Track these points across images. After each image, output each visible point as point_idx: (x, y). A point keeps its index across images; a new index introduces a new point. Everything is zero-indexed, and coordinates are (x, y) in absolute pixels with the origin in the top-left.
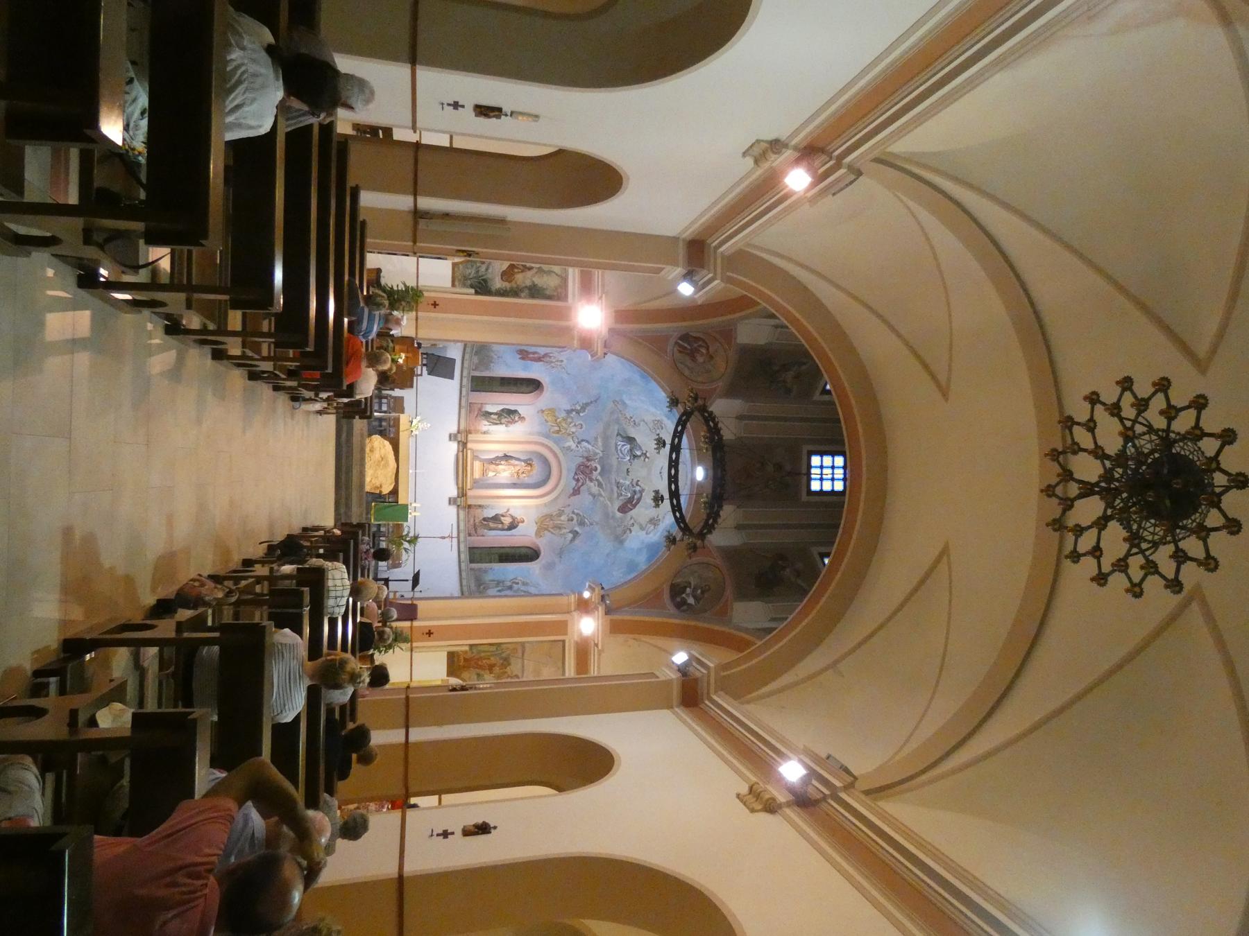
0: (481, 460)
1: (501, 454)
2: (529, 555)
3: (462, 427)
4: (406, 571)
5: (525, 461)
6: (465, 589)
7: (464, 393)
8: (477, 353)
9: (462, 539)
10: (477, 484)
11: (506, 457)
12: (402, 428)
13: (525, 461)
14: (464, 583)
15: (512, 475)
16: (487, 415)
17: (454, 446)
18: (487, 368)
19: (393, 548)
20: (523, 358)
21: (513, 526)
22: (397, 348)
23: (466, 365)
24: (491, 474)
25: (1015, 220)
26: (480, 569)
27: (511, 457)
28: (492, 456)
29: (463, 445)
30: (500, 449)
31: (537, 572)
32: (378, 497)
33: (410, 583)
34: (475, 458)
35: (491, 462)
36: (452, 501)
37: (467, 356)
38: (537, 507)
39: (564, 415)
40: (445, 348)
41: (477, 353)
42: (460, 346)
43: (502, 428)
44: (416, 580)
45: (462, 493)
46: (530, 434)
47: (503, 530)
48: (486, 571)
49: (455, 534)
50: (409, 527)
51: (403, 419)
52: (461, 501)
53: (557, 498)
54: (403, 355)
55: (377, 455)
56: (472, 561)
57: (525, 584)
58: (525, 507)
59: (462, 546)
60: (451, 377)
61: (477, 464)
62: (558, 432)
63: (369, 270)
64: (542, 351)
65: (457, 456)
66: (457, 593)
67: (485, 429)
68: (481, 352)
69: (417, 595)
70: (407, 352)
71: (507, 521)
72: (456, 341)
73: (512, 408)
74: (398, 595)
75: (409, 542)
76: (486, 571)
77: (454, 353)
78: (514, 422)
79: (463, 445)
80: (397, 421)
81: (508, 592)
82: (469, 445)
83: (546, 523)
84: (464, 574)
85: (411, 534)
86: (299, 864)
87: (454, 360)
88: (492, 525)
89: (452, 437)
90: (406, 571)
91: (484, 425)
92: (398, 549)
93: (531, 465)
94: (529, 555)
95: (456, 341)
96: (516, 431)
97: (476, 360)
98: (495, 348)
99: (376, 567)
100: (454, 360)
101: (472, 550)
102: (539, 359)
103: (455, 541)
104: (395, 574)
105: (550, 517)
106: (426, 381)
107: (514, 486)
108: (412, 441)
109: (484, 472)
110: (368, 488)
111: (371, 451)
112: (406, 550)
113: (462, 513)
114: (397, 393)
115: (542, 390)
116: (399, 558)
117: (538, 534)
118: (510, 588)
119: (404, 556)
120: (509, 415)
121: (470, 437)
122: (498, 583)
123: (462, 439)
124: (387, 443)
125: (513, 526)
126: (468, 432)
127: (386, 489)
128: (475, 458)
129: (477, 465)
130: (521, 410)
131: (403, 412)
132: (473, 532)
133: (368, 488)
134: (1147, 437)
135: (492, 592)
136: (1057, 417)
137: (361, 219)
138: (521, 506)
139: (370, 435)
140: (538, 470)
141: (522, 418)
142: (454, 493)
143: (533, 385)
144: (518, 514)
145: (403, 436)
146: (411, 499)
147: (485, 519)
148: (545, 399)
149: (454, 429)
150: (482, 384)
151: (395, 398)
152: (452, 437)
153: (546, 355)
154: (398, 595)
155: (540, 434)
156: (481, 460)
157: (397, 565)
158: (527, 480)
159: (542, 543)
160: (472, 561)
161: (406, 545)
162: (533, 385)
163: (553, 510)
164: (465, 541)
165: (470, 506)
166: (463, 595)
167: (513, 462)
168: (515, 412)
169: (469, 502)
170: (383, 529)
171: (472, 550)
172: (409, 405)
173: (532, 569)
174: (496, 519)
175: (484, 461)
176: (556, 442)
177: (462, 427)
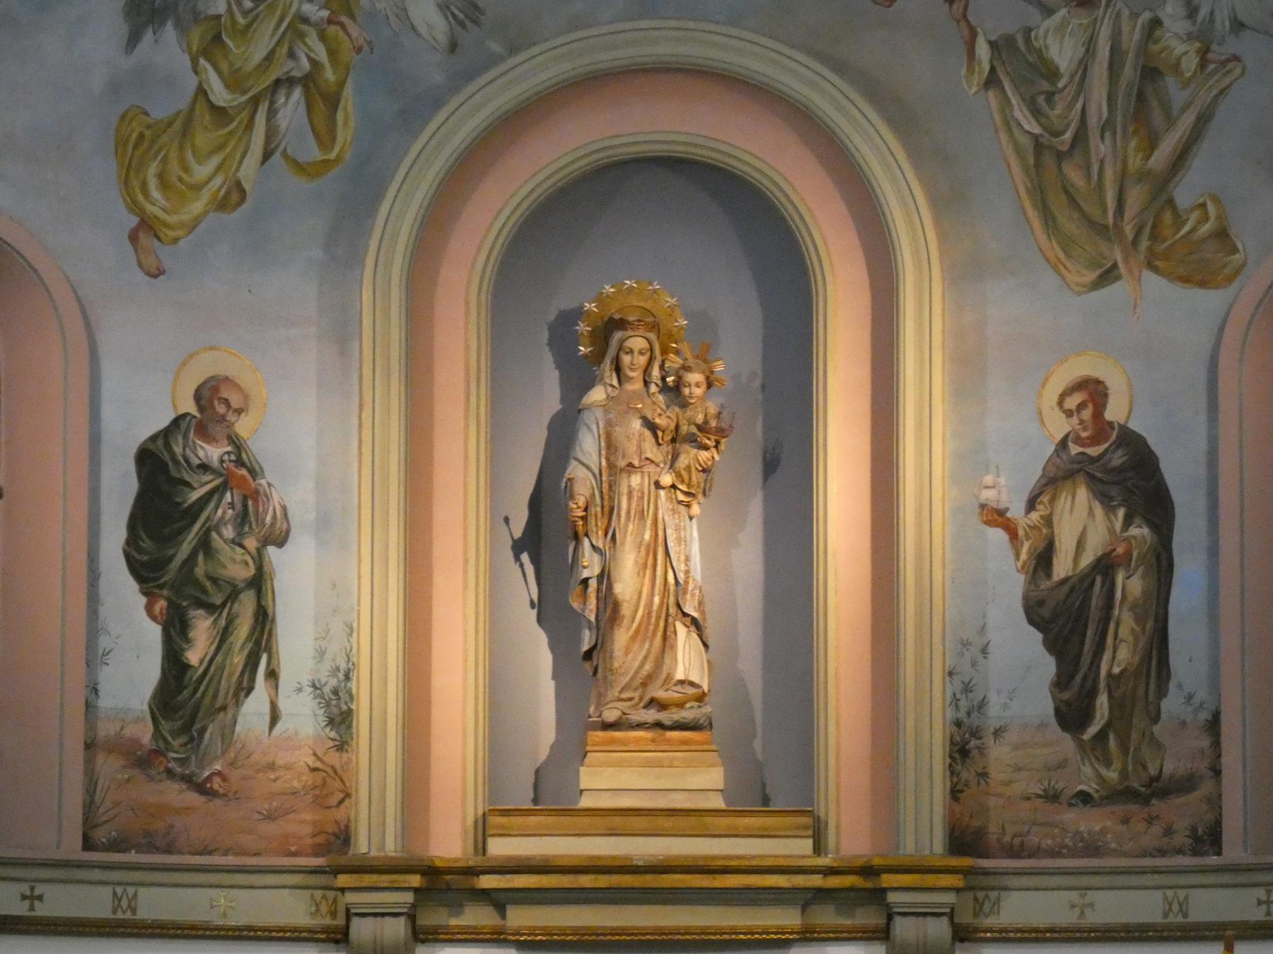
1: (522, 586)
5: (577, 380)
10: (774, 777)
11: (547, 535)
13: (577, 380)
15: (691, 490)
16: (184, 700)
25: (928, 825)
30: (476, 619)
34: (550, 796)
35: (583, 661)
38: (966, 272)
43: (296, 574)
46: (341, 333)
47: (1161, 566)
58: (969, 370)
61: (608, 779)
62: (323, 101)
67: (303, 717)
71: (1083, 526)
73: (120, 488)
82: (448, 843)
86: (1009, 124)
88: (1121, 655)
91: (278, 723)
93: (609, 327)
96: (317, 447)
107: (786, 466)
121: (377, 835)
125: (1128, 476)
128: (550, 796)
130: (140, 406)
132: (1182, 813)
134: (248, 558)
140: (648, 273)
141: (213, 405)
144: (1032, 428)
147: (1072, 716)
158: (740, 355)
165: (964, 840)
167: (582, 479)
168: (155, 463)
169: (924, 833)
174: (1066, 616)
175: (582, 728)
176: (416, 109)
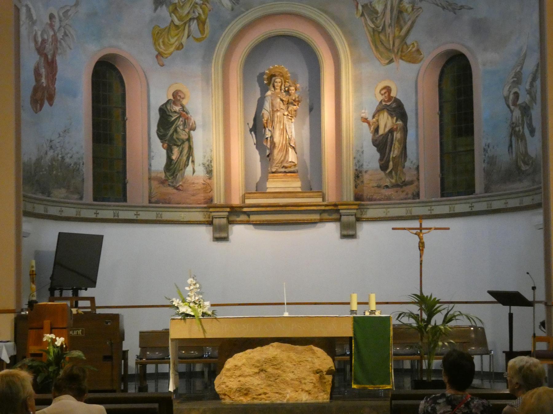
0: (264, 178)
1: (252, 139)
2: (456, 74)
3: (199, 216)
4: (492, 320)
5: (264, 89)
6: (527, 201)
7: (130, 215)
8: (46, 191)
9: (425, 211)
11: (258, 127)
12: (198, 335)
14: (513, 203)
15: (293, 115)
16: (172, 168)
17: (239, 232)
18: (76, 170)
19: (443, 346)
20: (51, 99)
21: (397, 110)
22: (33, 349)
23: (71, 212)
24: (292, 157)
26: (488, 174)
27: (258, 119)
28: (256, 156)
29: (236, 213)
30: (241, 144)
31: (491, 56)
32: (340, 376)
33: (515, 309)
34: (260, 189)
35: (267, 157)
36: (348, 232)
37: (53, 211)
38: (357, 61)
39: (164, 11)
40: (38, 255)
41: (46, 191)
42: (28, 225)
43: (198, 137)
44: (508, 298)
45: (331, 212)
46: (207, 79)
47: (405, 130)
48: (491, 161)
49: (415, 224)
50: (400, 314)
51: (179, 331)
52: (347, 214)
53: (341, 23)
54: (48, 337)
55: (255, 382)
56: (470, 189)
57: (517, 80)
58: (358, 83)
59: (438, 210)
60: (98, 240)
62: (202, 23)
63: (173, 340)
64: (30, 59)
65: (258, 224)
66: (538, 218)
67: (200, 172)
68: (39, 184)
69: (541, 295)
70: (41, 329)
71: (386, 122)
72: (19, 235)
73: (155, 117)
74: (540, 333)
75: (431, 315)
76: (491, 161)
77: (46, 236)
78: (184, 114)
79: (236, 213)
80: (185, 344)
81: (536, 112)
82: (236, 201)
83: (389, 39)
84: (497, 205)
85: (415, 309)
87: (62, 237)
88: (395, 152)
89: (221, 237)
90: (492, 320)
91: (194, 173)
92: (446, 335)
93: (272, 76)
94: (456, 74)
95: (19, 235)
97: (60, 193)
98: (30, 153)
99: (484, 375)
100: (62, 237)
101: (446, 191)
102: (51, 66)
103: (426, 224)
104: (496, 338)
105: (375, 33)
106: (108, 292)
107: (315, 109)
108: (221, 313)
109: (288, 171)
110: (323, 397)
111: (246, 392)
112: (447, 320)
113: (371, 213)
114: (131, 345)
115: (114, 57)
116: (462, 333)
117: (413, 57)
118: (526, 110)
119: (462, 322)
120: (171, 124)
121: (219, 199)
122: (515, 133)
123: (223, 217)
124: (230, 363)
125: (397, 110)
126: (209, 204)
127: (323, 360)
128: (260, 189)
129: (274, 184)
130: (159, 98)
131: (166, 333)
132: (410, 189)
133: (323, 397)
135: (533, 146)
136: (536, 290)
137: (124, 349)
138: (353, 97)
139: (216, 397)
140: (281, 60)
141: (177, 97)
142: (331, 229)
143: (107, 77)
144: (375, 98)
145: (214, 331)
146: (343, 312)
147: (384, 167)
148: (136, 53)
149: (204, 233)
150: (109, 179)
151: (144, 347)
152: (221, 237)
153: (40, 50)
154: (540, 333)
155: (207, 58)
156: (264, 178)
157: (479, 336)
158: (303, 82)
159: (432, 49)
160: (470, 189)
161: (438, 319)
162: (107, 77)
163: (363, 28)
164: (425, 203)
165: (358, 197)
166: (541, 205)
167: (266, 113)
168: (163, 111)
170: (407, 365)
171: (446, 191)
172: (152, 322)
173: (488, 67)
174: (382, 144)
175: (267, 173)
176: (224, 25)
177: (199, 216)
